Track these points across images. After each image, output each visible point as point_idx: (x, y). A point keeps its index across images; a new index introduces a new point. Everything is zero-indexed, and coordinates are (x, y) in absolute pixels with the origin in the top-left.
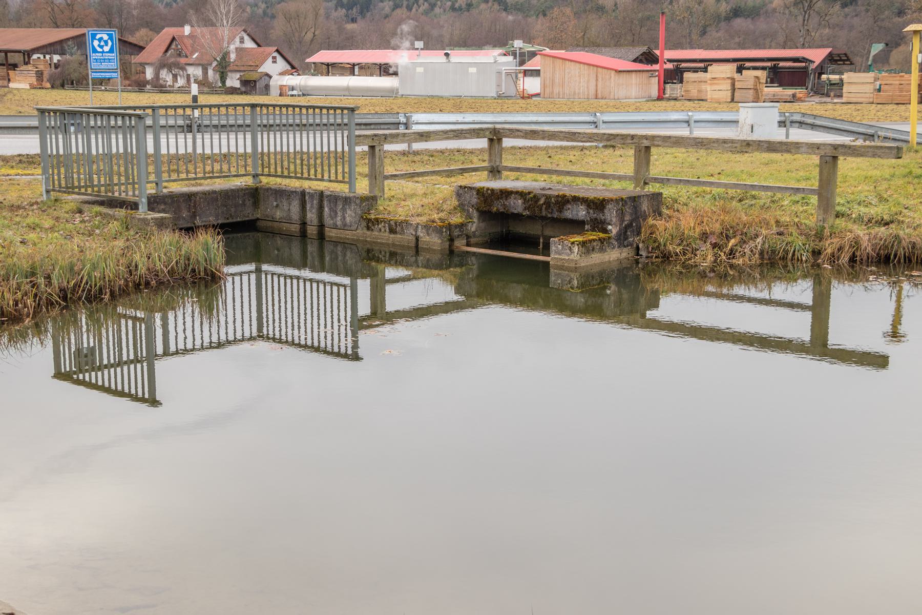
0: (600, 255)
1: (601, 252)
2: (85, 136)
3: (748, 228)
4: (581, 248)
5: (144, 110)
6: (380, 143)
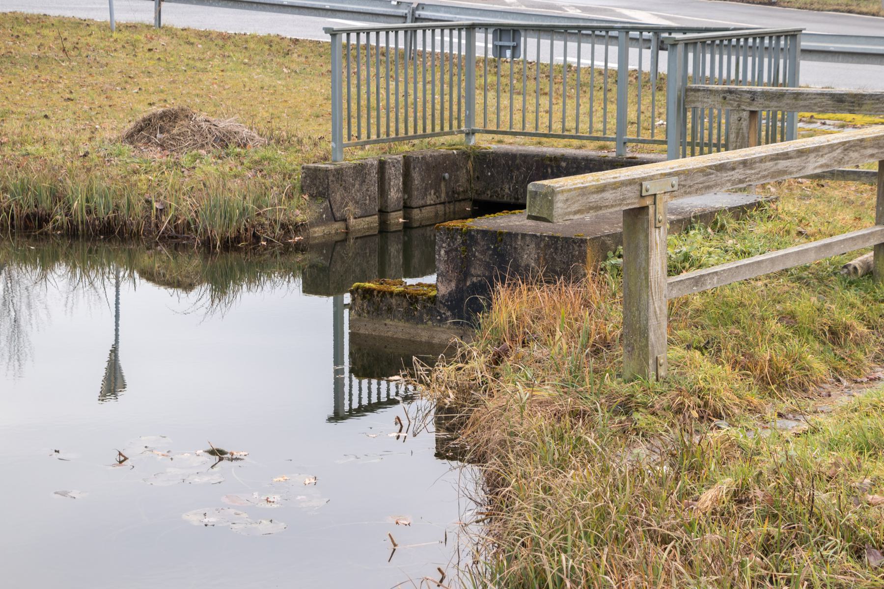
0: (407, 324)
1: (408, 321)
2: (773, 60)
3: (468, 324)
4: (359, 301)
5: (670, 34)
6: (739, 106)
